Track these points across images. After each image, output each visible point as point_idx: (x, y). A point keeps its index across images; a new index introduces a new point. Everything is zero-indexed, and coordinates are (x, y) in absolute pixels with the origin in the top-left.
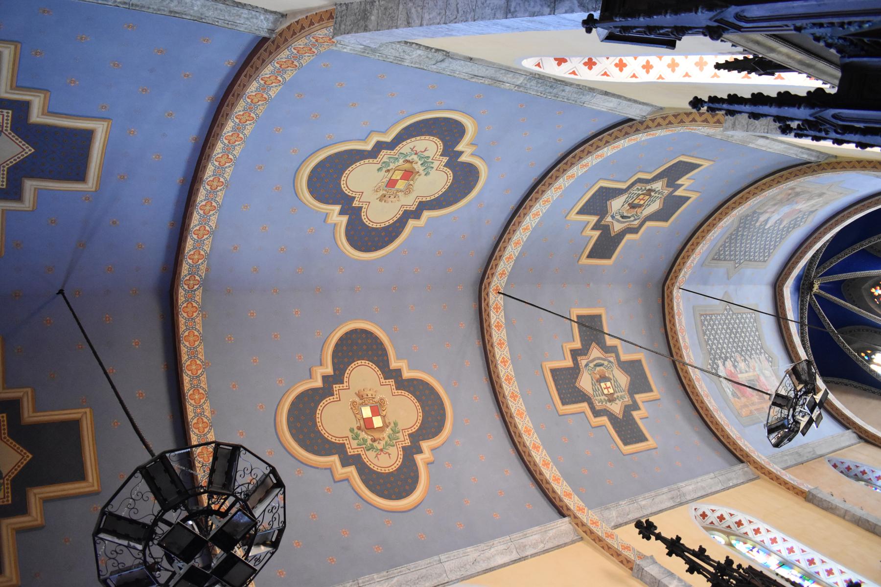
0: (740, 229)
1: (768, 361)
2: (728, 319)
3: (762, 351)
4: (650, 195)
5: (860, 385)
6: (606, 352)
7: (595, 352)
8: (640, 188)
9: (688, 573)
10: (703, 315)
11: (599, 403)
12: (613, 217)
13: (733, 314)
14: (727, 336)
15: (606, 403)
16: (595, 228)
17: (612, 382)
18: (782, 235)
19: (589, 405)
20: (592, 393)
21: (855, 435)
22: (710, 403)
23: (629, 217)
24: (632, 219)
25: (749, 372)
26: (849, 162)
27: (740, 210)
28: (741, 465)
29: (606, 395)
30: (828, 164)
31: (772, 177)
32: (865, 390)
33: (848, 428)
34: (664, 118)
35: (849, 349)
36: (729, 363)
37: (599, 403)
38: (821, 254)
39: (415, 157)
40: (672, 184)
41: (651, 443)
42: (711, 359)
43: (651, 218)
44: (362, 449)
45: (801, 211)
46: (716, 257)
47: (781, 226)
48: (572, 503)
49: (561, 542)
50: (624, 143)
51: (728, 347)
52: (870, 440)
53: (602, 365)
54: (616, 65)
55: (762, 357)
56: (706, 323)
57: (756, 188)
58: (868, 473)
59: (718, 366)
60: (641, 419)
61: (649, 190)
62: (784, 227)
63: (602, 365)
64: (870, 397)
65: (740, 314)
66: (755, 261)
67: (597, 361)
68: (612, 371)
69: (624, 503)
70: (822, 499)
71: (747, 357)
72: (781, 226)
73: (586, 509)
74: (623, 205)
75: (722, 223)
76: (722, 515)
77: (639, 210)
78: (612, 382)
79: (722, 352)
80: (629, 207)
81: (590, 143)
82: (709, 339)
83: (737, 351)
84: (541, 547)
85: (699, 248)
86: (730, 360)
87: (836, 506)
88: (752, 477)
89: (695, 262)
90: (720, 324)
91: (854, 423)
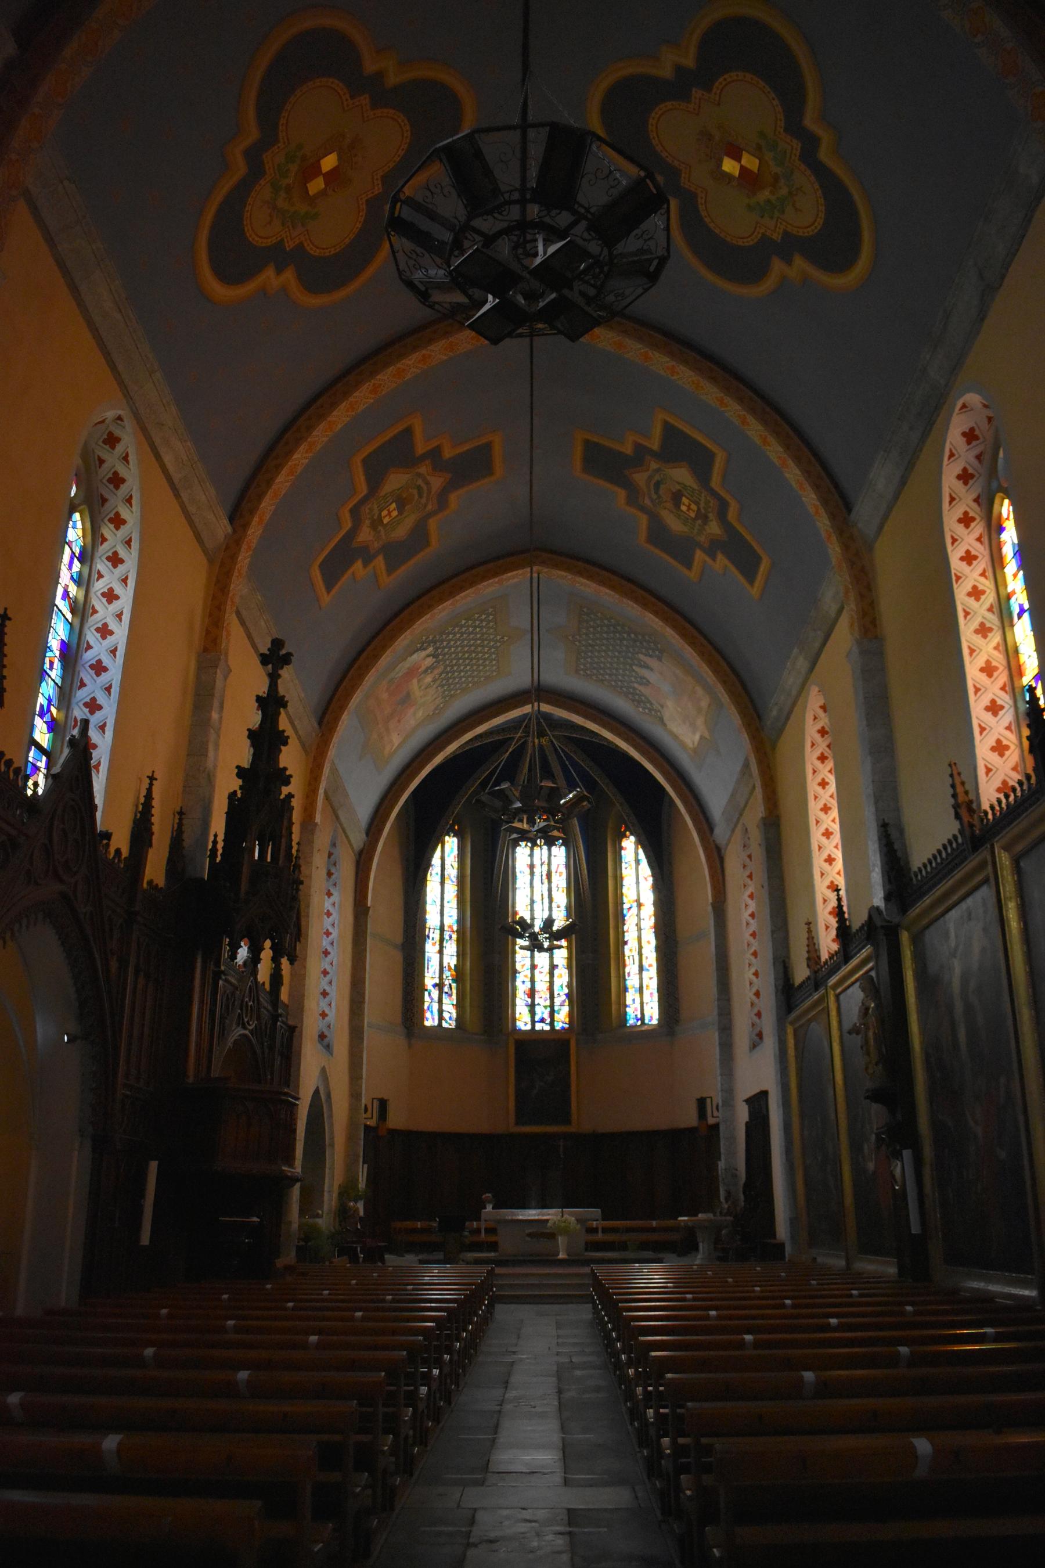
1: (436, 709)
3: (447, 698)
7: (437, 482)
12: (658, 470)
13: (497, 648)
16: (638, 446)
20: (381, 495)
23: (656, 493)
24: (655, 497)
28: (316, 725)
33: (367, 834)
37: (369, 509)
38: (588, 738)
39: (784, 191)
41: (326, 599)
43: (655, 519)
44: (273, 175)
45: (662, 706)
47: (636, 685)
50: (810, 498)
53: (420, 496)
54: (966, 513)
58: (331, 880)
59: (425, 649)
60: (374, 567)
62: (634, 689)
63: (420, 496)
67: (425, 487)
69: (260, 598)
70: (313, 842)
71: (438, 682)
72: (636, 685)
76: (819, 731)
77: (669, 505)
78: (400, 517)
79: (444, 648)
82: (462, 626)
83: (445, 668)
84: (192, 509)
85: (607, 591)
86: (435, 662)
90: (483, 634)
91: (377, 841)
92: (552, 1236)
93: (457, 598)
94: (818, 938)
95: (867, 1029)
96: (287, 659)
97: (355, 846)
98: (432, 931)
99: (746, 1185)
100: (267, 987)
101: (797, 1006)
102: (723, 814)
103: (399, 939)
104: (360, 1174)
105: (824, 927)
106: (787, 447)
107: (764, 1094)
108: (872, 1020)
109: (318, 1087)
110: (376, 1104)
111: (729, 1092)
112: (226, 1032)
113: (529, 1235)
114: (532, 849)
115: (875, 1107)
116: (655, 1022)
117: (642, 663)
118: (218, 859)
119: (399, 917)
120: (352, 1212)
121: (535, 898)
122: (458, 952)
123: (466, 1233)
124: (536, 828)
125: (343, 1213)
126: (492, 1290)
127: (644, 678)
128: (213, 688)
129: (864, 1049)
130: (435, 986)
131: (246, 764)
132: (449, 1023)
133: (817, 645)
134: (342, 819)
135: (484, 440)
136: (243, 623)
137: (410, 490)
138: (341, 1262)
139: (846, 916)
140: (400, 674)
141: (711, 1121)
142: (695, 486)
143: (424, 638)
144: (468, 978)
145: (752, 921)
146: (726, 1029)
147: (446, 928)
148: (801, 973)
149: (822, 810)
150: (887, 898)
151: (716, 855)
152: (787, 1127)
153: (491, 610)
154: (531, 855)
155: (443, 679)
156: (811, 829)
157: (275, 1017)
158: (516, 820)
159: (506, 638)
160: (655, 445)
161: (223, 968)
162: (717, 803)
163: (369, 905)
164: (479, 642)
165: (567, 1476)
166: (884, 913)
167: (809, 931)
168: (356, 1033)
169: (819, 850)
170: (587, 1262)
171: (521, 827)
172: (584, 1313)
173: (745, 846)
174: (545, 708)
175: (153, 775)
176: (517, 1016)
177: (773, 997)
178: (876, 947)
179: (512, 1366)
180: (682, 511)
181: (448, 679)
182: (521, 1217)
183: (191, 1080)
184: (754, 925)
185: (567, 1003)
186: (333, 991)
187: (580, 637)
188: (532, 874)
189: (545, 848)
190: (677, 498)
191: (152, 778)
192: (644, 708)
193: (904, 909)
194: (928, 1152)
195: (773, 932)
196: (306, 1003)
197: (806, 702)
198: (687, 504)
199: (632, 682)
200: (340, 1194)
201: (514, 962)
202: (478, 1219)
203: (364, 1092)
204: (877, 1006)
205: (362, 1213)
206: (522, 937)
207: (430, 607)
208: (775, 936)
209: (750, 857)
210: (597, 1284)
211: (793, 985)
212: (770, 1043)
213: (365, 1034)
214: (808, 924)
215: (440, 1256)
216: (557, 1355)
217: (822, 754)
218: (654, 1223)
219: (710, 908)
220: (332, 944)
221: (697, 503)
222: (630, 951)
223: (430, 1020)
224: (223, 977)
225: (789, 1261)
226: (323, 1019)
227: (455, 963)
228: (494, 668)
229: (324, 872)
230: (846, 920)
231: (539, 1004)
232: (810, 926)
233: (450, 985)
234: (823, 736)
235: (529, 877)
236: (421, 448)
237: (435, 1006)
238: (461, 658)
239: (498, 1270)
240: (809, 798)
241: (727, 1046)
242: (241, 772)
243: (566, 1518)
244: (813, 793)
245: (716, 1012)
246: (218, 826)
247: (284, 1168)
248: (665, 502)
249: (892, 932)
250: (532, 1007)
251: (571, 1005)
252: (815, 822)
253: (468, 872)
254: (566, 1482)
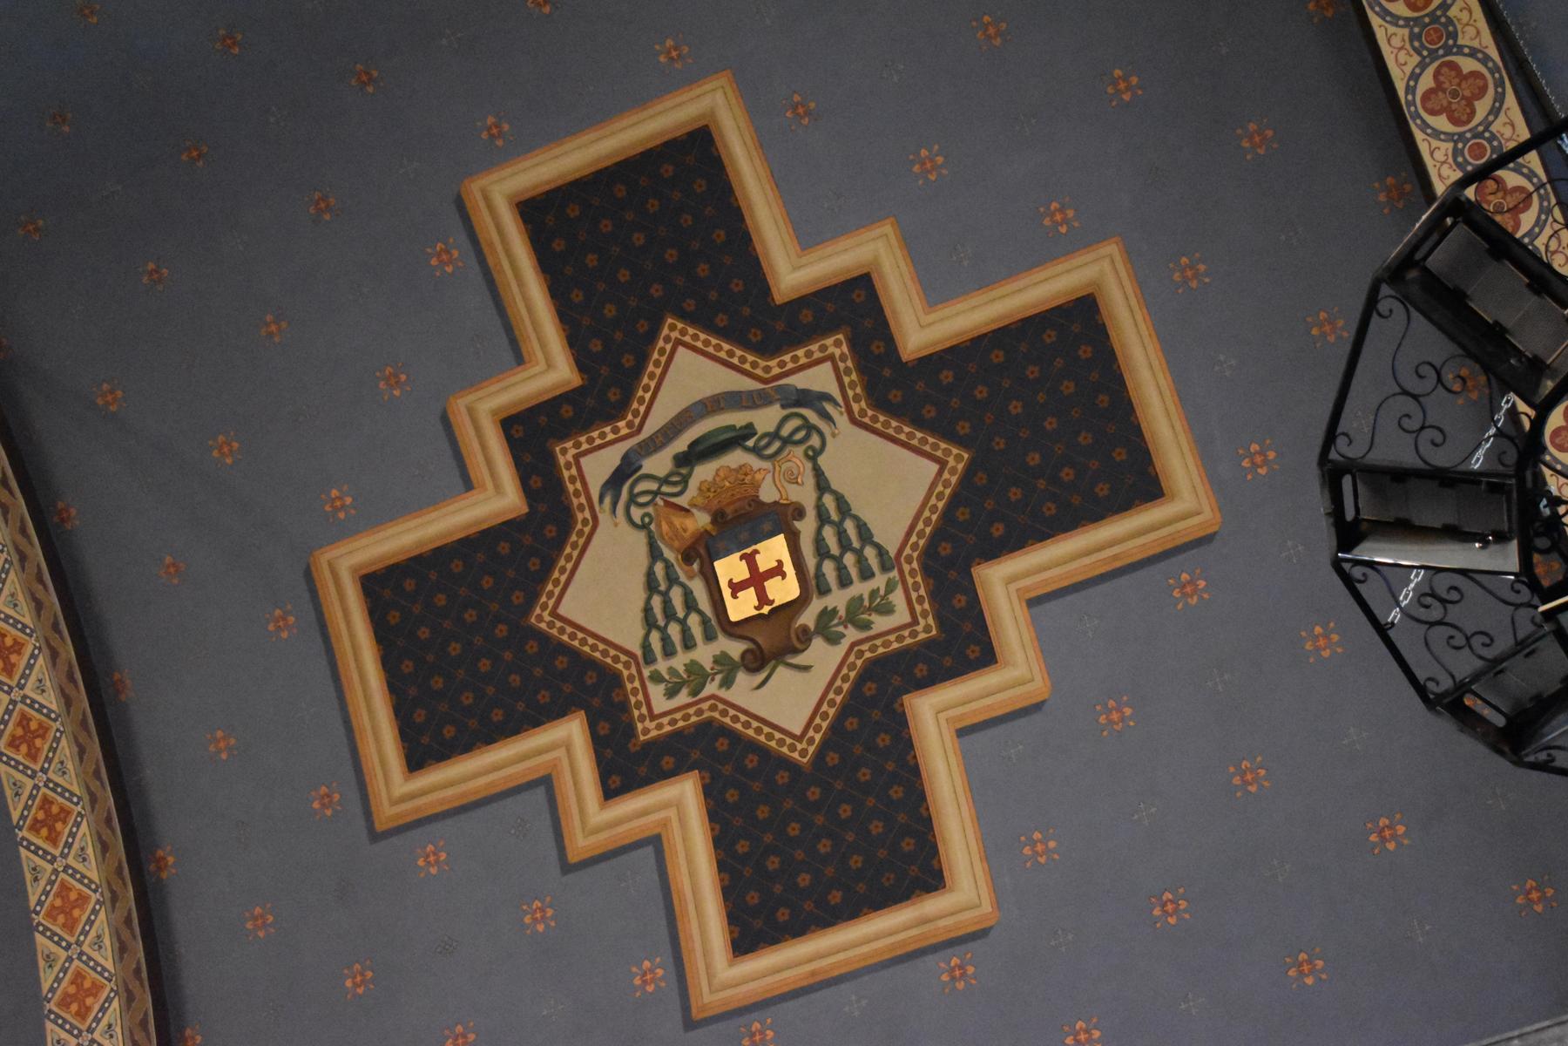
6: (767, 348)
8: (881, 623)
11: (671, 693)
23: (687, 460)
29: (734, 630)
37: (671, 693)
68: (813, 456)
74: (822, 485)
221: (811, 585)
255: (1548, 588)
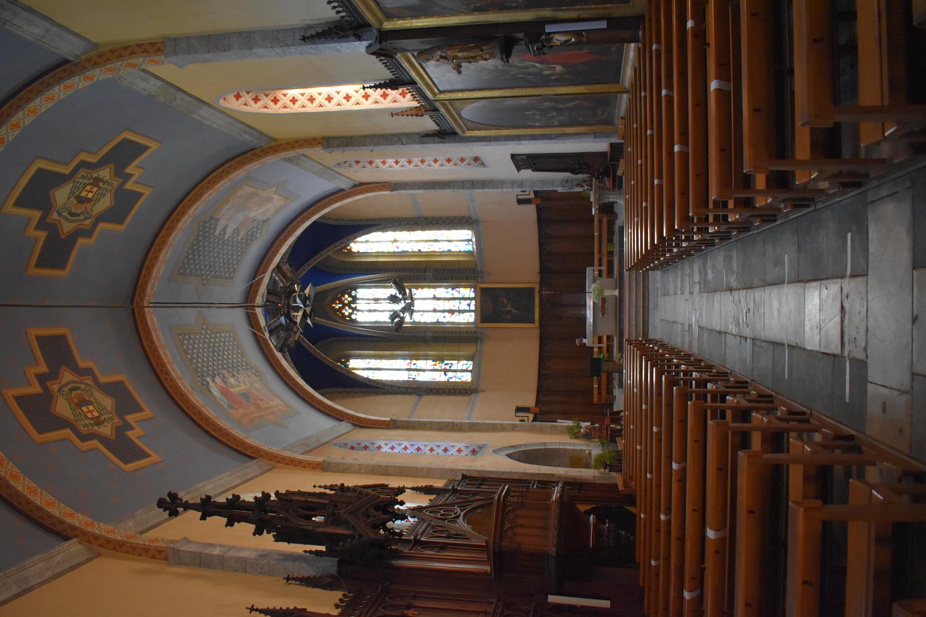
0: (200, 238)
1: (256, 375)
2: (207, 338)
4: (98, 186)
5: (343, 389)
7: (67, 376)
8: (85, 174)
9: (228, 527)
10: (181, 334)
11: (84, 427)
12: (59, 214)
14: (211, 354)
15: (93, 427)
17: (95, 404)
18: (242, 248)
19: (72, 430)
21: (350, 425)
22: (209, 412)
23: (78, 215)
24: (82, 217)
25: (240, 386)
26: (288, 144)
27: (196, 208)
28: (254, 461)
29: (90, 419)
30: (270, 148)
31: (220, 170)
32: (348, 392)
34: (100, 56)
35: (329, 360)
36: (218, 380)
37: (84, 427)
40: (121, 173)
41: (155, 457)
42: (199, 376)
46: (181, 271)
47: (240, 238)
48: (77, 521)
49: (74, 563)
50: (59, 92)
51: (214, 365)
52: (364, 425)
53: (79, 388)
55: (249, 372)
56: (186, 342)
57: (209, 182)
60: (135, 422)
61: (96, 178)
62: (242, 239)
63: (79, 388)
64: (354, 397)
65: (218, 333)
66: (221, 277)
67: (72, 385)
68: (66, 204)
70: (336, 463)
71: (235, 373)
73: (96, 523)
74: (69, 198)
75: (180, 225)
76: (256, 102)
77: (89, 206)
78: (95, 404)
80: (76, 202)
81: (19, 96)
82: (192, 357)
83: (225, 369)
84: (48, 574)
86: (219, 376)
87: (351, 464)
88: (268, 468)
89: (161, 272)
91: (347, 414)
92: (604, 300)
93: (166, 361)
94: (403, 108)
95: (456, 57)
96: (173, 496)
97: (350, 429)
98: (410, 376)
99: (574, 172)
100: (433, 497)
101: (452, 128)
102: (330, 181)
103: (414, 398)
104: (563, 424)
105: (394, 104)
106: (19, 108)
107: (513, 156)
108: (450, 53)
109: (506, 455)
110: (519, 414)
111: (513, 183)
112: (460, 533)
113: (603, 314)
114: (358, 311)
115: (514, 60)
116: (470, 232)
117: (222, 232)
118: (323, 548)
119: (400, 397)
120: (588, 431)
121: (368, 309)
122: (424, 360)
123: (602, 356)
124: (302, 306)
125: (588, 436)
126: (641, 341)
127: (234, 231)
128: (195, 553)
129: (471, 60)
130: (446, 375)
131: (252, 527)
132: (469, 365)
133: (187, 98)
134: (327, 439)
135: (35, 344)
136: (148, 529)
137: (72, 397)
138: (621, 444)
139: (382, 82)
140: (226, 400)
141: (532, 196)
142: (71, 185)
143: (199, 384)
144: (440, 353)
145: (401, 163)
146: (473, 184)
147: (409, 367)
148: (428, 124)
149: (312, 103)
150: (359, 38)
151: (359, 188)
152: (534, 138)
153: (181, 337)
154: (362, 311)
155: (233, 370)
156: (326, 110)
157: (454, 491)
158: (295, 320)
159: (204, 327)
160: (37, 215)
161: (412, 538)
162: (322, 186)
163: (389, 419)
164: (206, 345)
165: (849, 272)
166: (370, 42)
167: (397, 114)
168: (473, 427)
169: (340, 105)
170: (621, 275)
171: (300, 317)
172: (656, 277)
173: (350, 166)
174: (259, 300)
175: (249, 609)
176: (466, 321)
177: (447, 145)
178: (397, 50)
179: (703, 328)
180: (93, 196)
181: (233, 367)
182: (592, 320)
183: (488, 568)
184: (403, 161)
185: (458, 289)
186: (444, 445)
187: (203, 275)
188: (375, 311)
189: (357, 302)
190: (82, 200)
191: (252, 609)
192: (257, 233)
193: (368, 25)
194: (547, 13)
195: (402, 144)
196: (447, 466)
197: (231, 109)
198: (87, 193)
199: (238, 240)
200: (576, 438)
201: (432, 323)
202: (592, 348)
203: (511, 422)
204: (439, 49)
205: (588, 424)
206: (403, 318)
207: (172, 380)
208: (404, 143)
209: (357, 162)
210: (636, 266)
211: (438, 131)
212: (479, 150)
213: (475, 421)
214: (392, 115)
215: (616, 375)
216: (692, 293)
217: (272, 101)
218: (596, 234)
219: (395, 193)
220: (412, 445)
221: (85, 185)
222: (425, 247)
223: (467, 377)
224: (419, 537)
225: (622, 139)
226: (462, 451)
227: (431, 361)
228: (227, 335)
229: (363, 452)
230: (385, 82)
231: (459, 307)
232: (394, 113)
233: (445, 365)
234: (259, 100)
235: (377, 313)
236: (36, 389)
237: (459, 374)
238: (218, 358)
239: (626, 336)
240: (304, 111)
241: (484, 184)
242: (258, 532)
243: (859, 280)
244: (300, 109)
245: (462, 191)
246: (299, 548)
247: (554, 499)
248: (86, 208)
249: (384, 36)
250: (460, 311)
251: (459, 287)
252: (321, 108)
253: (372, 352)
254: (860, 273)
255: (823, 439)
